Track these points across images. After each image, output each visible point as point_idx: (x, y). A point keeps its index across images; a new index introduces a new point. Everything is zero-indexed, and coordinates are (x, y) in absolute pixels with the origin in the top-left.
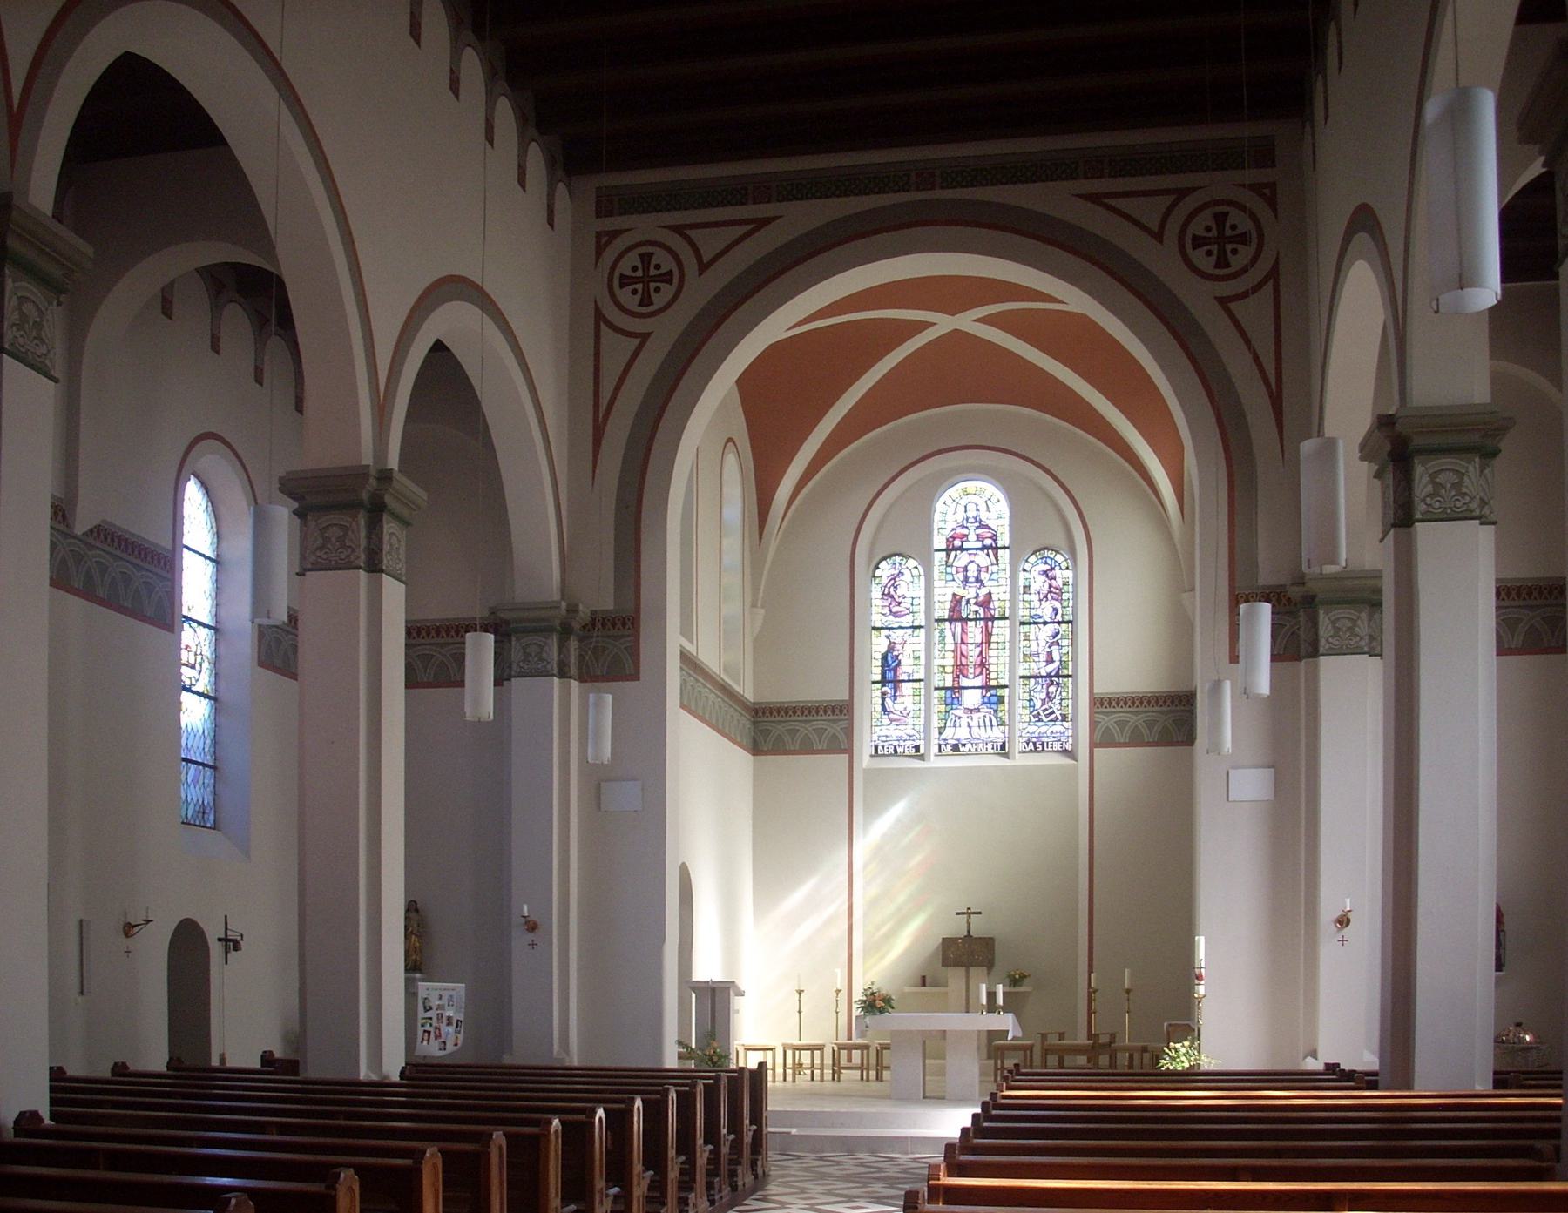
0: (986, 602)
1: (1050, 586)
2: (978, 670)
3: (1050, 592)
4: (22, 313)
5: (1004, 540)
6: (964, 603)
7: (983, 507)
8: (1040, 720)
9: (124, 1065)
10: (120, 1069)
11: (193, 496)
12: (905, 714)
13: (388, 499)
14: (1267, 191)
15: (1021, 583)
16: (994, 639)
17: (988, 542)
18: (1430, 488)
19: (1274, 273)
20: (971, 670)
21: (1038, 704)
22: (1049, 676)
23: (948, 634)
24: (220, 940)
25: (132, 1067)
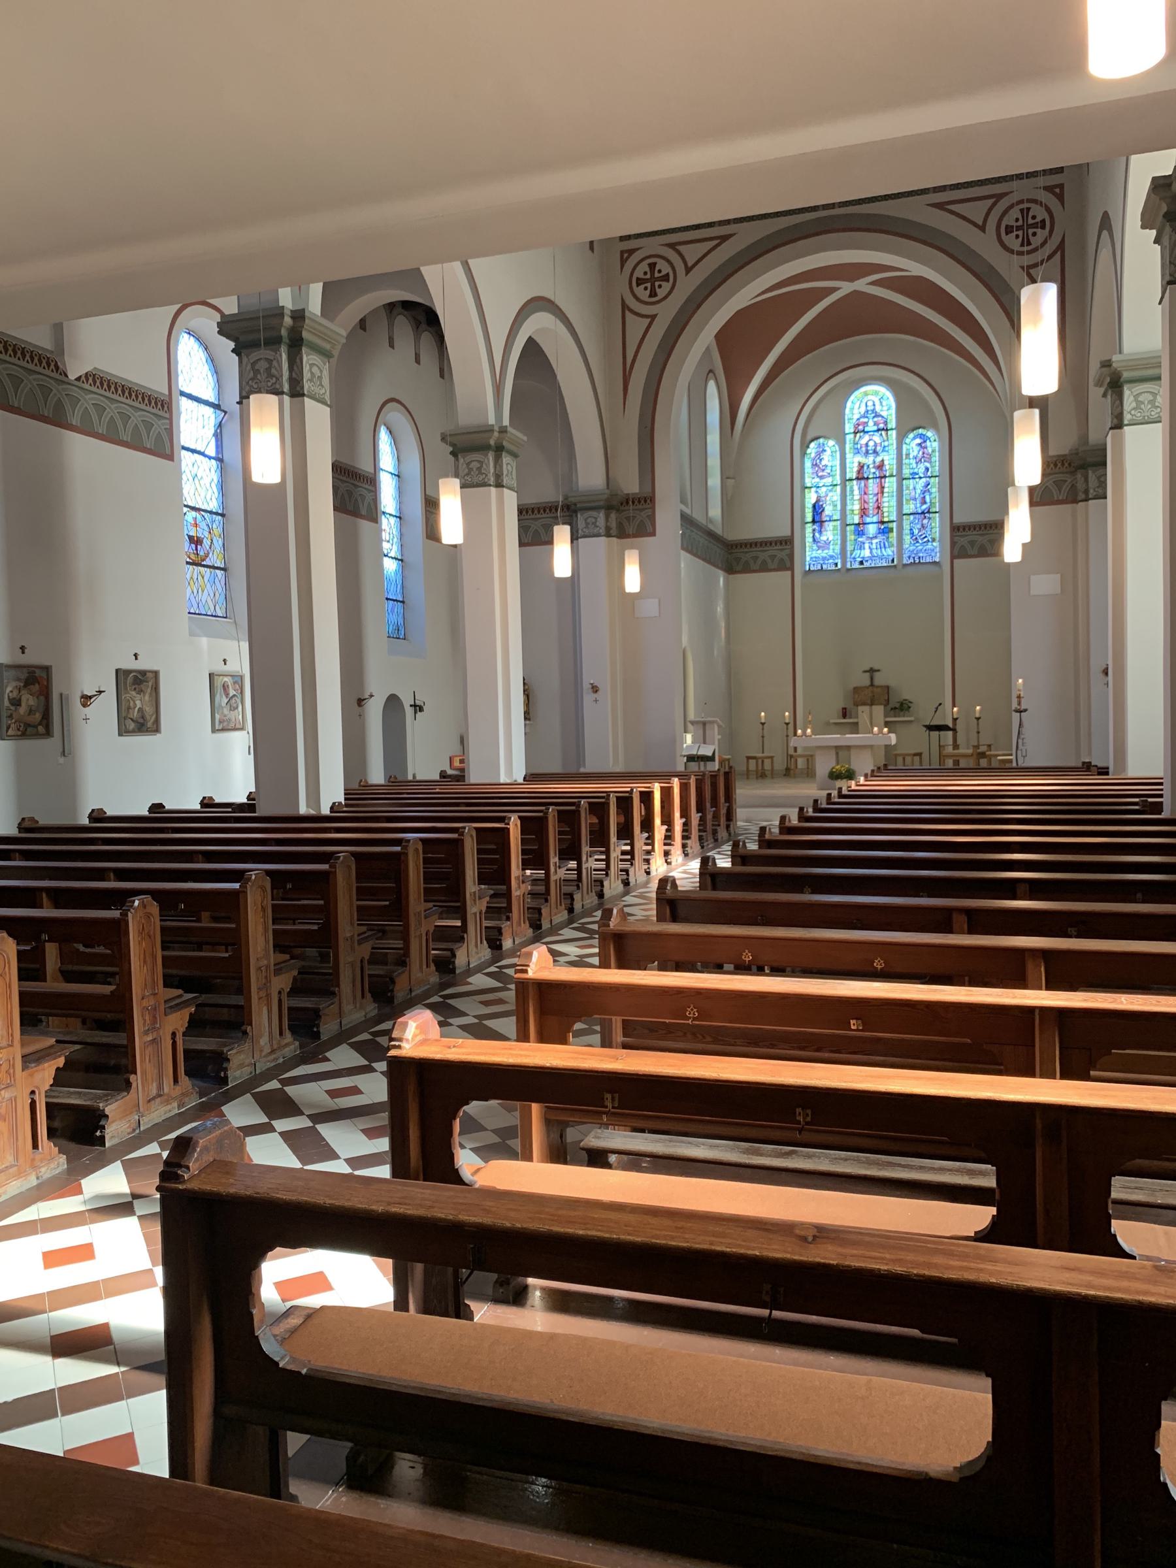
0: (881, 466)
1: (924, 453)
2: (876, 511)
3: (924, 457)
4: (312, 373)
5: (892, 424)
6: (865, 468)
7: (877, 403)
8: (918, 542)
9: (161, 806)
10: (207, 803)
11: (384, 437)
12: (827, 543)
13: (505, 443)
14: (1057, 190)
15: (904, 452)
16: (886, 490)
17: (881, 426)
18: (1134, 405)
19: (1061, 247)
20: (871, 512)
21: (916, 532)
22: (923, 513)
23: (856, 488)
24: (411, 706)
25: (110, 812)
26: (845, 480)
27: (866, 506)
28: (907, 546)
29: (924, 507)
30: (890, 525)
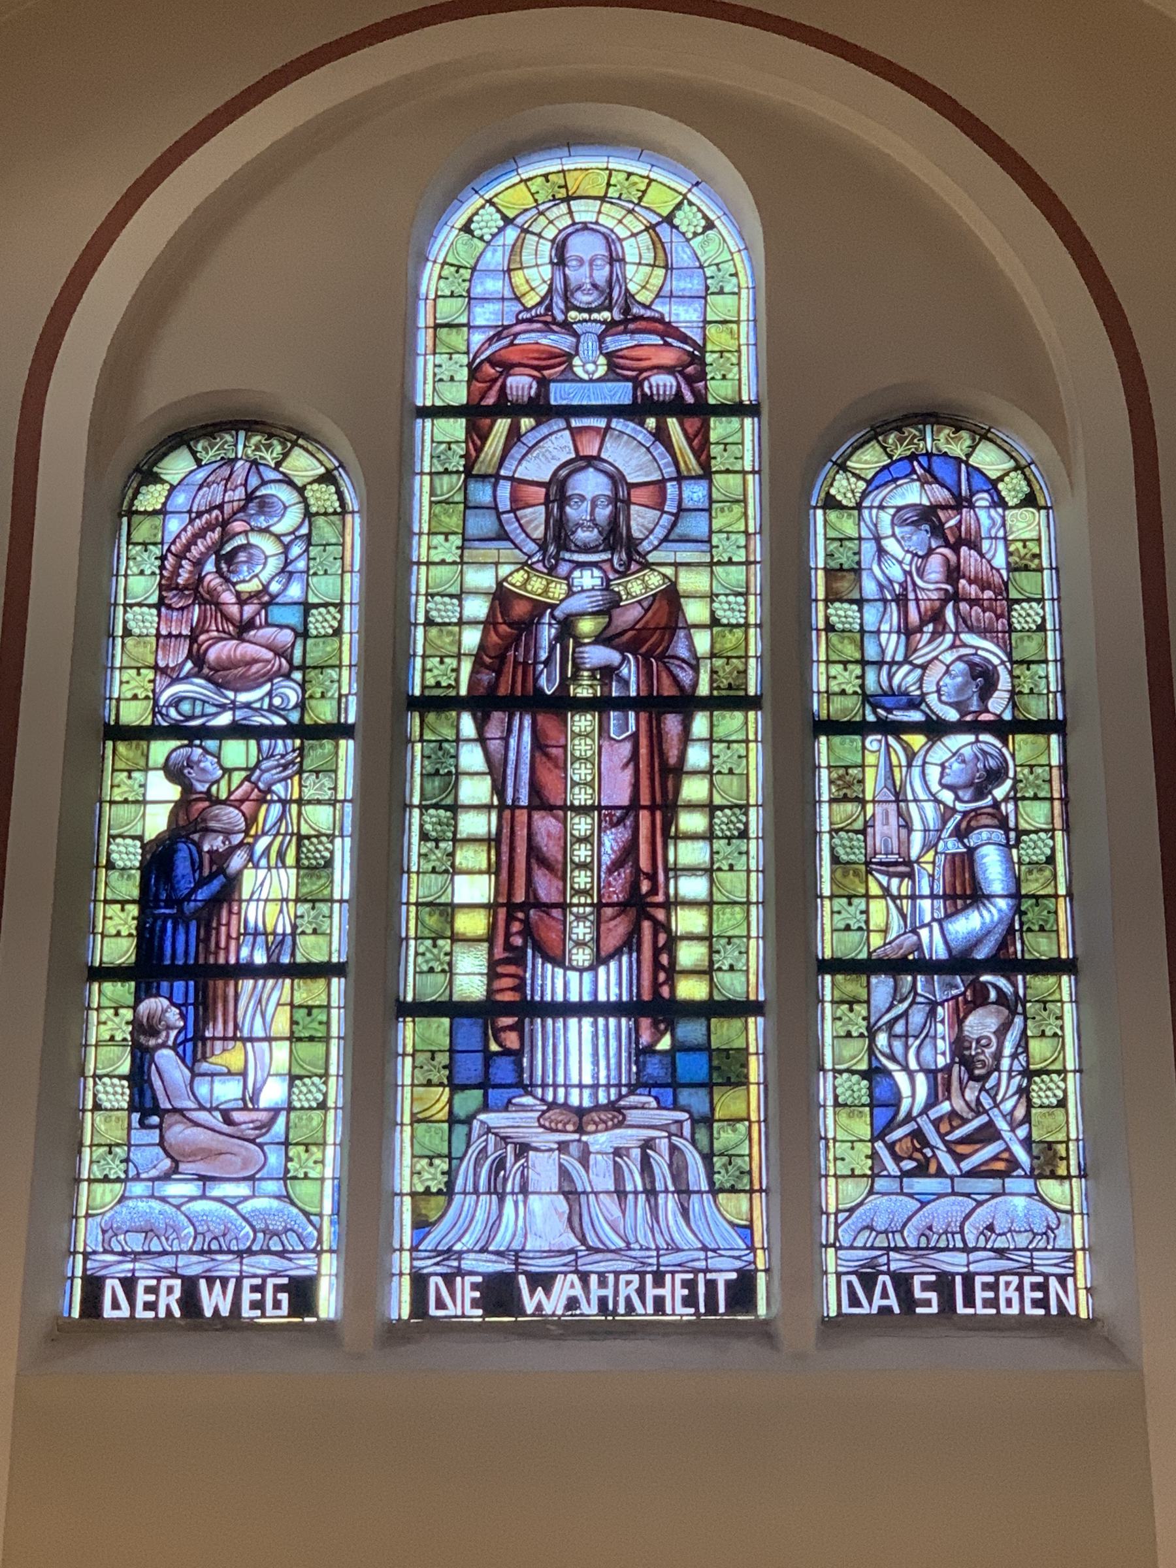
1: (953, 573)
6: (547, 633)
7: (636, 249)
17: (663, 384)
26: (343, 572)
27: (546, 888)
28: (853, 1191)
29: (968, 924)
30: (725, 1032)
